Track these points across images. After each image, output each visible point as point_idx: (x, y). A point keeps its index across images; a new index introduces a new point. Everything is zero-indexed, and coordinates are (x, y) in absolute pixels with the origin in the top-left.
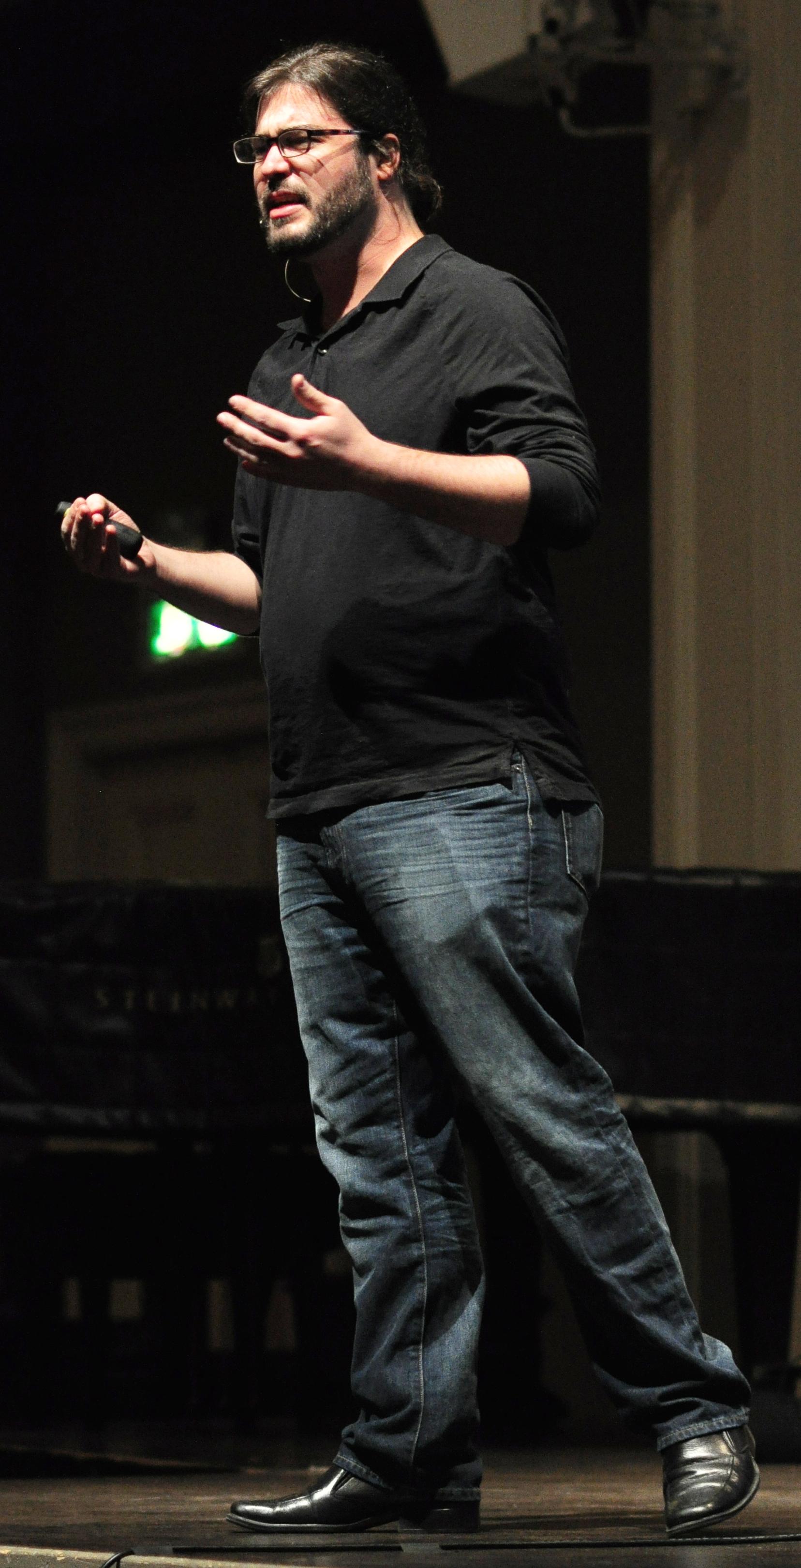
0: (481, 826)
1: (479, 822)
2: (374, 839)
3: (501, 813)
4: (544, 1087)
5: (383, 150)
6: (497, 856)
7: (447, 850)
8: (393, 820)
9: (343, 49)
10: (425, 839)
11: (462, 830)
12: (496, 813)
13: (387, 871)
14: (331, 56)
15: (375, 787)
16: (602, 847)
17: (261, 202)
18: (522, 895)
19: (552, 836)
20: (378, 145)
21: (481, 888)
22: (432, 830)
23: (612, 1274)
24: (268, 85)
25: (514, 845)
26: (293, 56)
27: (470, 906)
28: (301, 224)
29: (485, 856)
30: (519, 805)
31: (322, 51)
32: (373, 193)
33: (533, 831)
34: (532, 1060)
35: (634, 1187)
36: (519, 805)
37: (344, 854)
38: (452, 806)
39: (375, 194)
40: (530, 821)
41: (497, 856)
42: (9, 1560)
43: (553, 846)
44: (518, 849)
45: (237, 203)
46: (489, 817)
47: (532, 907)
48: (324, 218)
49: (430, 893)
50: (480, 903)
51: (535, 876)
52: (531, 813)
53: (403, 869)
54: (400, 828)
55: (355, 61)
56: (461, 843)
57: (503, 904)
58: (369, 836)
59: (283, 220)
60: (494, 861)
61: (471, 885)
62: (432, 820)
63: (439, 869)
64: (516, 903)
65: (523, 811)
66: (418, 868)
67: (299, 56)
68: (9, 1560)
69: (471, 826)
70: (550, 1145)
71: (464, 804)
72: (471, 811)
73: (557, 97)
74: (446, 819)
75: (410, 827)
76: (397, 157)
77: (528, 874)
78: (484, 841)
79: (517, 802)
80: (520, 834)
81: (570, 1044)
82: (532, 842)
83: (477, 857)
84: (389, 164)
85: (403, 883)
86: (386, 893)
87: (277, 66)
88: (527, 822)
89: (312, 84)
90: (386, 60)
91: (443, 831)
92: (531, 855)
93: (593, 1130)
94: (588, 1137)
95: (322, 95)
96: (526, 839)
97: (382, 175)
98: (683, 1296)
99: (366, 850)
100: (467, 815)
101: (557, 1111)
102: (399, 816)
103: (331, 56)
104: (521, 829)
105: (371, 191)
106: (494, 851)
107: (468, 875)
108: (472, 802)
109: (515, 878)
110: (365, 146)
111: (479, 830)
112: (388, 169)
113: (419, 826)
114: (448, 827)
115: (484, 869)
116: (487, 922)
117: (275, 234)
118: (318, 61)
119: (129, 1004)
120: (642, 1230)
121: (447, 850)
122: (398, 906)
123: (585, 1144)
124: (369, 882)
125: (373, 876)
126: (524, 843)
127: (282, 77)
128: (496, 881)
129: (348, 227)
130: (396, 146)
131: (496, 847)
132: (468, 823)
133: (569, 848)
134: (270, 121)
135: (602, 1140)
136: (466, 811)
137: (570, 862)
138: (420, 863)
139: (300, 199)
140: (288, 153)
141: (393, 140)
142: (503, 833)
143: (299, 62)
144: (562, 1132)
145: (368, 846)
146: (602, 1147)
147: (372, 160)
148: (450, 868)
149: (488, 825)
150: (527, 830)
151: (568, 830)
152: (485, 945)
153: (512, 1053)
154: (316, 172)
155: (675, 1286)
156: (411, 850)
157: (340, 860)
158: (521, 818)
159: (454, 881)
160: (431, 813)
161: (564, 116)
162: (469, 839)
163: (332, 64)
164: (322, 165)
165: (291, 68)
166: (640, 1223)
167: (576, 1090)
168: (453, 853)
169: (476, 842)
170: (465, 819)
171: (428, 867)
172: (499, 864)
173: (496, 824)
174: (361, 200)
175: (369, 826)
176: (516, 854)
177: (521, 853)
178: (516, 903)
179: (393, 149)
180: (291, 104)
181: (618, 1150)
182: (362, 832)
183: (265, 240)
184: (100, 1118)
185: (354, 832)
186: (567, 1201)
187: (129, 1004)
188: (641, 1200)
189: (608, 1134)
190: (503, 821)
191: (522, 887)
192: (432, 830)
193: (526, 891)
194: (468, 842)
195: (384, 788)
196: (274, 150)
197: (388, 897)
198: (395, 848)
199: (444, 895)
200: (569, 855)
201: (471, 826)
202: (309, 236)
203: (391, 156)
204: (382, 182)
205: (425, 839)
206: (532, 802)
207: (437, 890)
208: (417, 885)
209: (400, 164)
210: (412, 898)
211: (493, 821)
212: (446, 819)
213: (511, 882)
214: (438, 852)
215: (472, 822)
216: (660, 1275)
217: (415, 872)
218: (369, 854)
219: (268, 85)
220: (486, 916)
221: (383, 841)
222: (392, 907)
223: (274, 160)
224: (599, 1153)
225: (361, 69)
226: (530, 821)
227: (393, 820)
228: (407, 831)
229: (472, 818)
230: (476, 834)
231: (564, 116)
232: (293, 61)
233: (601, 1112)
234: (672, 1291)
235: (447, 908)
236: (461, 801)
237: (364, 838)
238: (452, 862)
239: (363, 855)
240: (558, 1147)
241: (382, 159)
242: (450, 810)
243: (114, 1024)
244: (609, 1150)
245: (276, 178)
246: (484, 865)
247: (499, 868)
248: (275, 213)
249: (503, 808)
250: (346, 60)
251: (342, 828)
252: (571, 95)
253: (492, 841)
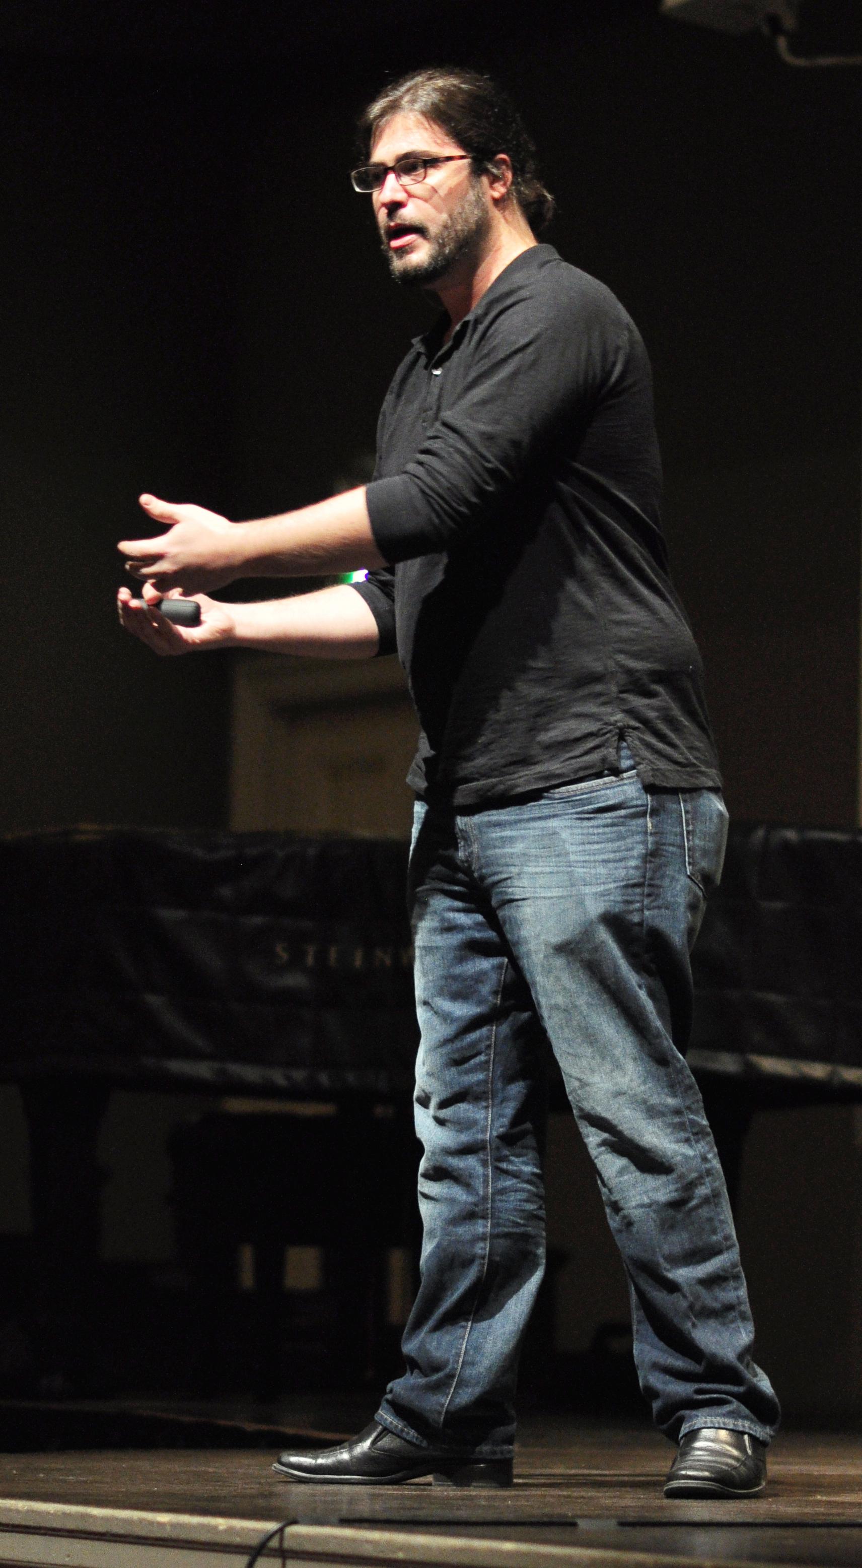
0: (600, 830)
1: (598, 827)
2: (502, 838)
3: (621, 817)
4: (643, 1088)
5: (495, 171)
6: (615, 861)
7: (567, 854)
8: (520, 821)
9: (451, 73)
10: (546, 842)
11: (583, 834)
12: (616, 817)
13: (512, 869)
14: (440, 83)
15: (494, 786)
16: (724, 848)
17: (382, 232)
18: (638, 898)
19: (670, 839)
20: (490, 166)
21: (596, 893)
22: (554, 834)
23: (682, 1274)
24: (382, 114)
25: (632, 849)
26: (401, 85)
27: (585, 913)
28: (420, 255)
29: (604, 861)
30: (638, 809)
31: (430, 79)
32: (487, 212)
33: (651, 834)
34: (635, 1059)
35: (714, 1196)
36: (638, 809)
37: (475, 848)
38: (574, 811)
39: (490, 214)
40: (650, 825)
41: (615, 861)
42: (168, 1528)
43: (671, 849)
44: (635, 853)
45: (363, 235)
46: (609, 821)
47: (648, 909)
48: (442, 246)
49: (549, 895)
50: (595, 908)
51: (651, 879)
52: (651, 816)
53: (526, 869)
54: (525, 829)
55: (463, 86)
56: (580, 848)
57: (617, 910)
58: (499, 834)
59: (402, 251)
60: (611, 865)
61: (587, 890)
62: (553, 823)
63: (558, 872)
64: (632, 907)
65: (643, 814)
66: (538, 870)
67: (409, 84)
68: (168, 1528)
69: (591, 831)
70: (642, 1143)
71: (586, 808)
72: (592, 816)
73: (774, 22)
74: (568, 823)
75: (535, 828)
76: (509, 175)
77: (644, 877)
78: (603, 845)
79: (637, 806)
80: (638, 838)
81: (672, 1050)
82: (650, 846)
83: (595, 861)
84: (502, 183)
85: (525, 882)
86: (510, 890)
87: (387, 96)
88: (646, 827)
89: (424, 113)
90: (491, 79)
91: (565, 835)
92: (649, 858)
93: (683, 1135)
94: (678, 1141)
95: (431, 123)
96: (645, 843)
97: (496, 195)
98: (743, 1308)
99: (495, 847)
100: (589, 819)
101: (652, 1112)
102: (525, 817)
103: (440, 83)
104: (639, 833)
105: (485, 211)
106: (612, 856)
107: (584, 880)
108: (592, 806)
109: (631, 882)
110: (478, 169)
111: (598, 834)
112: (499, 190)
113: (542, 829)
114: (569, 831)
115: (600, 874)
116: (601, 927)
117: (398, 264)
118: (425, 89)
119: (310, 960)
120: (715, 1238)
121: (567, 854)
122: (520, 903)
123: (674, 1146)
124: (496, 878)
125: (501, 873)
126: (642, 847)
127: (394, 107)
128: (612, 886)
129: (468, 247)
130: (507, 166)
131: (615, 852)
132: (588, 827)
133: (689, 849)
134: (384, 152)
135: (691, 1146)
136: (587, 816)
137: (690, 864)
138: (541, 864)
139: (419, 230)
140: (406, 180)
141: (503, 161)
142: (621, 837)
143: (408, 90)
144: (653, 1132)
145: (497, 844)
146: (691, 1153)
147: (485, 180)
148: (568, 873)
149: (607, 830)
150: (646, 833)
151: (688, 832)
152: (598, 948)
153: (617, 1052)
154: (431, 198)
155: (738, 1298)
156: (533, 852)
157: (472, 853)
158: (640, 821)
159: (572, 885)
160: (554, 816)
161: (782, 43)
162: (589, 843)
163: (441, 90)
164: (436, 192)
165: (401, 97)
166: (714, 1232)
167: (674, 1095)
168: (572, 857)
169: (596, 846)
170: (586, 823)
171: (548, 869)
172: (616, 868)
173: (615, 829)
174: (477, 222)
175: (499, 825)
176: (633, 857)
177: (639, 857)
178: (632, 907)
179: (504, 167)
180: (405, 128)
181: (705, 1159)
182: (492, 829)
183: (388, 269)
184: (278, 1077)
185: (485, 830)
186: (649, 1197)
187: (310, 960)
188: (719, 1210)
189: (697, 1141)
190: (623, 824)
191: (638, 890)
192: (554, 834)
193: (642, 894)
194: (587, 847)
195: (502, 787)
196: (391, 178)
197: (512, 894)
198: (519, 847)
199: (561, 897)
200: (689, 857)
201: (591, 831)
202: (430, 264)
203: (503, 174)
204: (496, 202)
205: (546, 842)
206: (652, 806)
207: (556, 892)
208: (537, 886)
209: (513, 183)
210: (534, 898)
211: (613, 825)
212: (568, 823)
213: (626, 886)
214: (558, 856)
215: (592, 827)
216: (724, 1284)
217: (537, 873)
218: (497, 851)
219: (382, 114)
220: (599, 922)
221: (511, 840)
222: (515, 903)
223: (391, 189)
224: (686, 1157)
225: (469, 93)
226: (650, 825)
227: (520, 821)
228: (531, 832)
229: (592, 823)
230: (596, 838)
231: (782, 43)
232: (403, 89)
233: (693, 1120)
234: (735, 1301)
235: (564, 910)
236: (584, 805)
237: (494, 835)
238: (570, 866)
239: (490, 852)
240: (648, 1146)
241: (494, 179)
242: (572, 814)
243: (295, 980)
244: (695, 1156)
245: (394, 207)
246: (602, 870)
247: (617, 872)
248: (395, 243)
249: (623, 812)
250: (454, 86)
251: (475, 824)
252: (789, 22)
253: (610, 846)
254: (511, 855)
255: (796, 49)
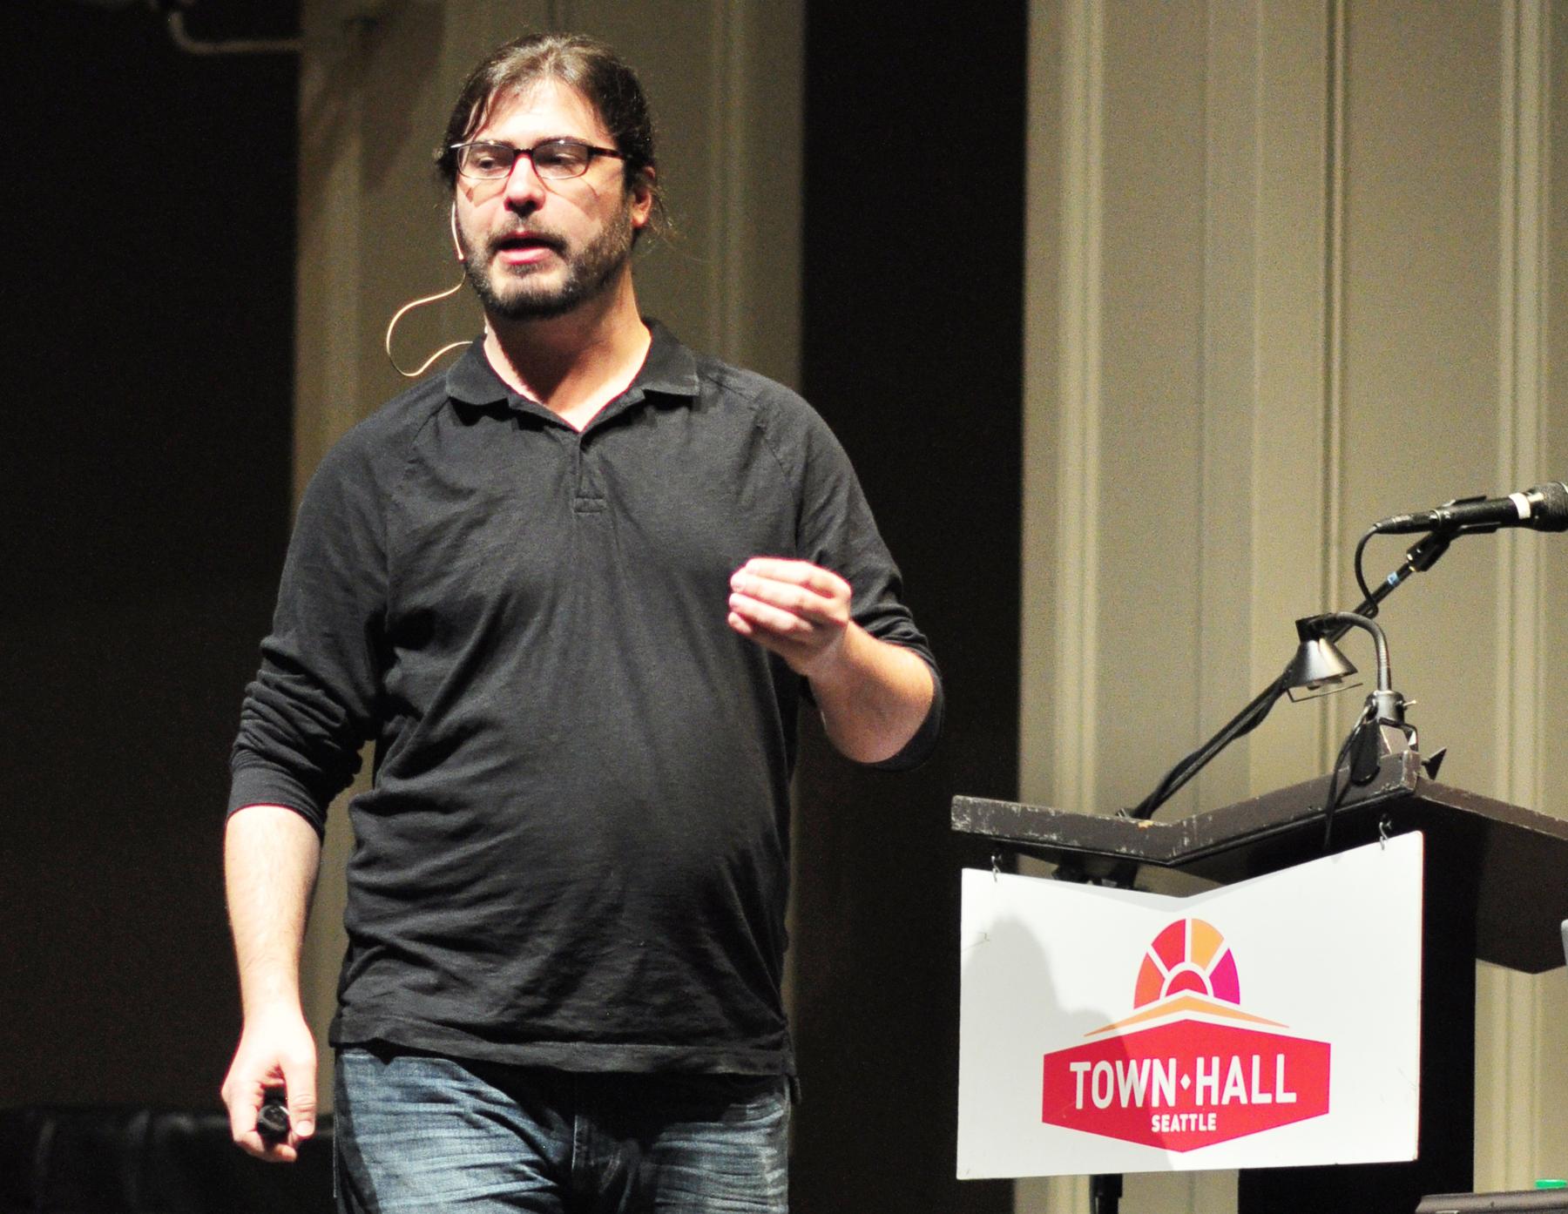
127: (533, 65)
161: (175, 21)
165: (545, 56)
195: (696, 1060)
196: (524, 164)
231: (175, 21)
254: (688, 1177)
255: (193, 30)
